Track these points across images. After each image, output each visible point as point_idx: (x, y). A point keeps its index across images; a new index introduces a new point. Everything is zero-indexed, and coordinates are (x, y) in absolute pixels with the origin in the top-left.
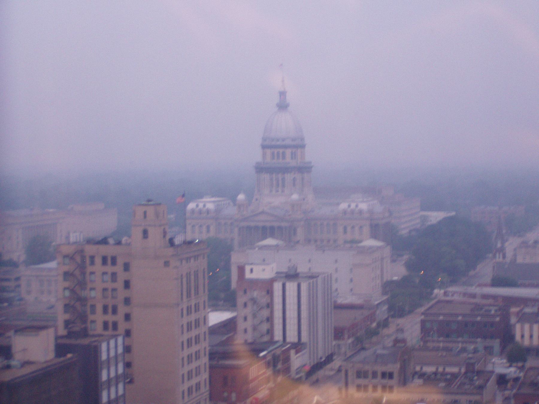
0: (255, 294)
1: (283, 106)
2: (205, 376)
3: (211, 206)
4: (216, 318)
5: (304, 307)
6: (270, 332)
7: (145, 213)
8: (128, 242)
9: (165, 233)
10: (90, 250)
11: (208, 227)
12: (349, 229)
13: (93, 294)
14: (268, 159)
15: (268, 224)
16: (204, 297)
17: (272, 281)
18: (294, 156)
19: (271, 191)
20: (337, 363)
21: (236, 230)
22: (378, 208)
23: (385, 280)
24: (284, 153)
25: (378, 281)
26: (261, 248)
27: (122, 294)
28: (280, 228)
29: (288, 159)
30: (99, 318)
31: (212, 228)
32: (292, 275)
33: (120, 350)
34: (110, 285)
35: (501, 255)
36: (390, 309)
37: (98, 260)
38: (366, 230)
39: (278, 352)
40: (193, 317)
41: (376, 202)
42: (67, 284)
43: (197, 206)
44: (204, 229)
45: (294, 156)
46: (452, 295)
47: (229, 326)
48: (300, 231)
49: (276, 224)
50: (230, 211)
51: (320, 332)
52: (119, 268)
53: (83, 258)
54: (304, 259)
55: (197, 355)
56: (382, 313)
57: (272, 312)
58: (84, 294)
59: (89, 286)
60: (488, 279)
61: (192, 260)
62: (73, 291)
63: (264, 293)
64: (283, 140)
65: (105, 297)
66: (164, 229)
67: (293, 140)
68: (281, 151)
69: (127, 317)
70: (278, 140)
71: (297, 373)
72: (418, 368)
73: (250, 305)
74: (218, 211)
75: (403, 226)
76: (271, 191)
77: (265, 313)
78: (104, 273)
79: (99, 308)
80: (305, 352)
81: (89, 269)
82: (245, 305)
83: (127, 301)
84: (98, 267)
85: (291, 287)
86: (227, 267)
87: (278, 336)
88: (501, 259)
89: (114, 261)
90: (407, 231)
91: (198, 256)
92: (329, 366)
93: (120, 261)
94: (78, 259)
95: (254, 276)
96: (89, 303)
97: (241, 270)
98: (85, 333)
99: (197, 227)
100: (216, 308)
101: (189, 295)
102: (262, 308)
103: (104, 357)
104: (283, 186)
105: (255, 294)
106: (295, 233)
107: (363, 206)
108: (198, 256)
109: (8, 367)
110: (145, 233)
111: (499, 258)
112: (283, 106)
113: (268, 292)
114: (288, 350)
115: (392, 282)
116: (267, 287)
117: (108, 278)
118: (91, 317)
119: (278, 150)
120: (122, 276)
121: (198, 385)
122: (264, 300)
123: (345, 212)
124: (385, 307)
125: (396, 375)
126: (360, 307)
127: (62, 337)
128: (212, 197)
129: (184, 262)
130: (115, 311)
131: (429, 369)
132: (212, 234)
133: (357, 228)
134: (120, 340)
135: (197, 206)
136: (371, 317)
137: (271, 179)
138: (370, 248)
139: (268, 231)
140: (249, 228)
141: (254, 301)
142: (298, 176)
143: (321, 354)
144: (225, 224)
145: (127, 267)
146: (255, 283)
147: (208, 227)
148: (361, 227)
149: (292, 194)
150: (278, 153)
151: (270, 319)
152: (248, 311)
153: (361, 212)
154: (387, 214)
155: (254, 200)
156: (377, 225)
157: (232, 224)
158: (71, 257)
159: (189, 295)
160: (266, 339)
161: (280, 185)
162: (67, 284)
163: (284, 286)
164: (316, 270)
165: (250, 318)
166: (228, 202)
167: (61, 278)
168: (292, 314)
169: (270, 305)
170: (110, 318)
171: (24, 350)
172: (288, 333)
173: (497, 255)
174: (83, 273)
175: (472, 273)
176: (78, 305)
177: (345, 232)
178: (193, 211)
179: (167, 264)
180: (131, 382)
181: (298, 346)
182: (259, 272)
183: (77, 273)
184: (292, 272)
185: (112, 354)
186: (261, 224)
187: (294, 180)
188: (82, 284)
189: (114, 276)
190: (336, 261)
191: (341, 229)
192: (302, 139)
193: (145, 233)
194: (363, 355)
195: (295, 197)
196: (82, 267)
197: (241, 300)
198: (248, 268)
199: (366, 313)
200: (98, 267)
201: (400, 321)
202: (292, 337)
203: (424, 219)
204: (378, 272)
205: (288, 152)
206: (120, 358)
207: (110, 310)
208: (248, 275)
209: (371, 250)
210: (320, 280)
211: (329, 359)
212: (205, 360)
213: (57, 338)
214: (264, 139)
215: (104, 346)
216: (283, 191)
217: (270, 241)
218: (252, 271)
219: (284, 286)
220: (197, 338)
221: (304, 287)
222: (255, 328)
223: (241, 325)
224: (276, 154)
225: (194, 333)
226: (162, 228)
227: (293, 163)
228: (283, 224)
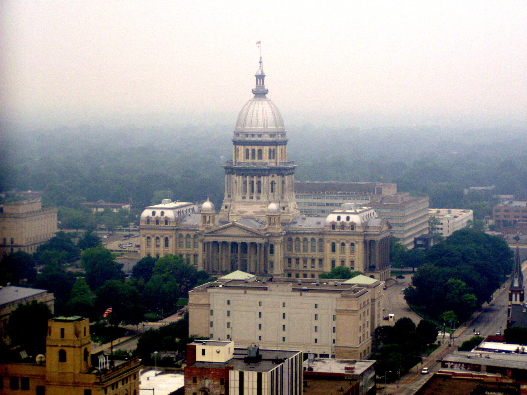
0: (207, 383)
1: (260, 93)
3: (170, 214)
7: (62, 330)
8: (43, 359)
11: (167, 240)
12: (338, 246)
14: (241, 158)
15: (239, 240)
18: (272, 154)
19: (244, 198)
21: (200, 245)
23: (376, 326)
24: (260, 151)
25: (368, 330)
28: (254, 244)
29: (266, 159)
31: (171, 241)
35: (518, 296)
43: (154, 213)
44: (162, 242)
45: (272, 154)
46: (452, 367)
49: (248, 241)
50: (194, 220)
61: (120, 386)
64: (260, 136)
67: (272, 135)
68: (257, 148)
70: (253, 135)
74: (179, 219)
75: (406, 235)
76: (244, 198)
88: (518, 302)
91: (126, 378)
95: (206, 359)
99: (153, 240)
104: (259, 191)
105: (207, 383)
106: (272, 252)
107: (355, 219)
108: (126, 378)
110: (63, 356)
111: (516, 300)
112: (260, 93)
119: (253, 147)
123: (333, 226)
128: (173, 201)
129: (109, 390)
132: (171, 250)
133: (348, 246)
135: (154, 213)
137: (245, 183)
138: (361, 286)
140: (215, 243)
142: (277, 179)
144: (188, 236)
147: (167, 240)
148: (352, 244)
149: (270, 202)
150: (253, 151)
154: (385, 228)
155: (223, 208)
156: (372, 242)
157: (195, 236)
163: (241, 375)
166: (191, 207)
173: (514, 296)
177: (333, 250)
186: (230, 240)
187: (273, 183)
190: (316, 306)
191: (328, 246)
192: (283, 134)
195: (273, 206)
203: (434, 222)
204: (368, 318)
205: (266, 149)
210: (286, 365)
214: (237, 134)
216: (259, 198)
219: (241, 375)
221: (266, 377)
224: (250, 152)
226: (83, 348)
227: (272, 164)
228: (258, 241)
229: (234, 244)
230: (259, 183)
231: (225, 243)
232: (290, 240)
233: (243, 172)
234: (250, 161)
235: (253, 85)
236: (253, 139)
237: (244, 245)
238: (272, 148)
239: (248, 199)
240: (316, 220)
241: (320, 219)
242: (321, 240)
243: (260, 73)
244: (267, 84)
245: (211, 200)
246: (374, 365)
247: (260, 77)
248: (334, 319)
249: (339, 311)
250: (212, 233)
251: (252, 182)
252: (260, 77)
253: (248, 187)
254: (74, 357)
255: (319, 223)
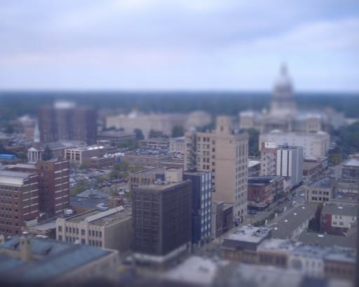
2: (246, 190)
4: (252, 163)
5: (290, 158)
6: (275, 171)
10: (199, 134)
13: (199, 153)
16: (246, 156)
17: (277, 149)
20: (305, 186)
26: (273, 134)
27: (212, 154)
30: (202, 163)
32: (286, 147)
33: (210, 178)
34: (207, 150)
36: (329, 162)
37: (202, 139)
38: (319, 127)
39: (278, 181)
40: (242, 164)
42: (189, 149)
47: (257, 167)
51: (297, 163)
52: (210, 143)
53: (195, 138)
54: (291, 139)
55: (243, 188)
56: (325, 165)
57: (276, 163)
58: (196, 153)
59: (198, 150)
62: (191, 152)
65: (204, 154)
69: (213, 164)
71: (286, 190)
72: (340, 190)
73: (266, 160)
77: (273, 163)
78: (204, 145)
79: (202, 160)
80: (290, 180)
81: (198, 143)
82: (264, 159)
83: (213, 157)
84: (202, 142)
85: (285, 152)
86: (257, 141)
87: (278, 173)
89: (208, 140)
92: (300, 187)
93: (211, 140)
94: (193, 138)
95: (269, 147)
96: (197, 157)
97: (263, 144)
98: (195, 170)
100: (252, 159)
101: (240, 155)
102: (271, 161)
103: (203, 181)
105: (269, 155)
109: (163, 184)
114: (282, 180)
115: (330, 150)
116: (274, 152)
117: (206, 147)
118: (198, 163)
120: (212, 146)
121: (243, 194)
122: (273, 157)
124: (326, 162)
125: (330, 194)
126: (315, 161)
127: (186, 171)
130: (208, 161)
131: (345, 191)
134: (210, 174)
136: (320, 166)
139: (275, 126)
141: (269, 157)
143: (297, 182)
145: (214, 143)
146: (269, 150)
151: (275, 166)
152: (264, 162)
158: (191, 138)
159: (240, 155)
160: (273, 174)
162: (189, 149)
164: (296, 145)
165: (266, 165)
167: (186, 146)
168: (285, 164)
169: (275, 160)
170: (206, 164)
171: (170, 177)
172: (283, 172)
174: (195, 145)
176: (192, 157)
179: (231, 142)
180: (215, 191)
181: (287, 178)
182: (271, 145)
183: (193, 144)
185: (207, 180)
188: (195, 149)
189: (208, 146)
194: (316, 183)
196: (195, 142)
197: (263, 157)
198: (266, 144)
199: (318, 164)
200: (202, 142)
201: (333, 168)
202: (285, 174)
206: (210, 182)
207: (206, 160)
208: (266, 146)
209: (321, 136)
210: (298, 150)
211: (301, 184)
212: (246, 183)
213: (184, 172)
215: (203, 177)
217: (276, 131)
218: (268, 145)
220: (243, 174)
222: (268, 169)
223: (262, 168)
225: (241, 172)
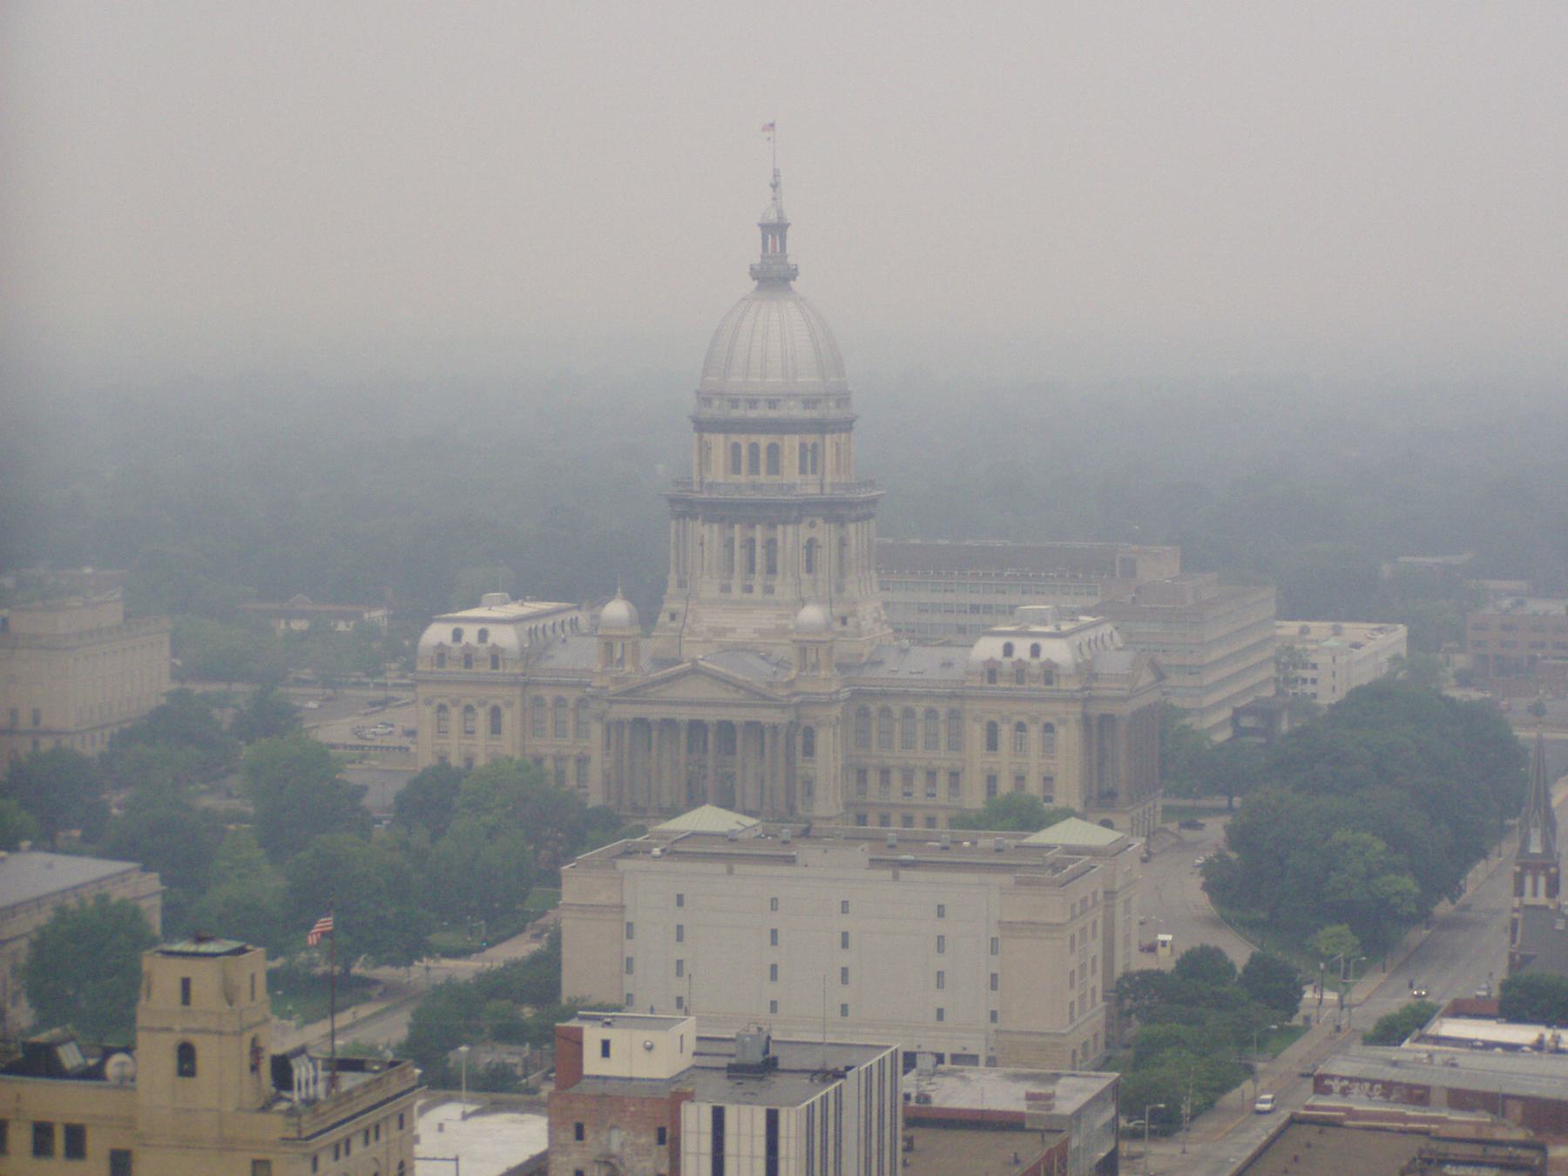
0: (616, 1140)
1: (774, 277)
7: (186, 983)
8: (128, 1070)
9: (256, 1051)
11: (496, 713)
12: (1005, 732)
14: (718, 472)
15: (710, 716)
17: (674, 1096)
18: (810, 460)
19: (726, 589)
21: (597, 730)
22: (1117, 661)
23: (1119, 971)
24: (774, 450)
25: (1096, 982)
28: (755, 728)
29: (790, 472)
35: (1542, 881)
41: (1108, 628)
43: (457, 635)
44: (482, 719)
45: (810, 460)
46: (1345, 1092)
48: (825, 740)
49: (738, 716)
50: (577, 656)
60: (1486, 982)
61: (357, 1146)
63: (648, 1139)
64: (772, 404)
66: (254, 1041)
67: (810, 403)
68: (763, 441)
70: (753, 404)
74: (534, 651)
76: (726, 589)
88: (1542, 899)
90: (1226, 713)
95: (613, 1067)
99: (455, 713)
105: (616, 1140)
106: (809, 750)
107: (1057, 651)
110: (186, 1058)
111: (1535, 894)
112: (774, 277)
113: (661, 1139)
119: (754, 438)
123: (992, 671)
128: (516, 597)
132: (509, 745)
133: (1034, 732)
137: (729, 544)
140: (641, 723)
142: (825, 533)
144: (559, 702)
147: (496, 713)
148: (1049, 728)
149: (803, 602)
153: (1050, 673)
154: (1146, 678)
155: (664, 618)
156: (1107, 721)
157: (581, 703)
161: (758, 567)
173: (1529, 880)
175: (1443, 908)
178: (441, 654)
184: (755, 1057)
186: (683, 715)
191: (976, 734)
193: (186, 1058)
195: (812, 614)
203: (1291, 661)
204: (1096, 948)
205: (791, 444)
214: (705, 399)
216: (769, 590)
224: (744, 452)
226: (248, 1036)
227: (809, 488)
228: (768, 716)
229: (697, 727)
230: (771, 544)
231: (669, 724)
232: (864, 713)
233: (722, 512)
234: (743, 478)
235: (753, 253)
236: (753, 414)
237: (726, 728)
238: (811, 439)
239: (736, 592)
240: (940, 654)
241: (953, 653)
242: (954, 715)
243: (773, 217)
244: (797, 249)
245: (628, 597)
246: (1115, 1086)
247: (775, 230)
248: (994, 950)
249: (1007, 927)
250: (632, 694)
251: (751, 542)
252: (775, 230)
253: (739, 555)
254: (221, 1062)
255: (948, 664)
